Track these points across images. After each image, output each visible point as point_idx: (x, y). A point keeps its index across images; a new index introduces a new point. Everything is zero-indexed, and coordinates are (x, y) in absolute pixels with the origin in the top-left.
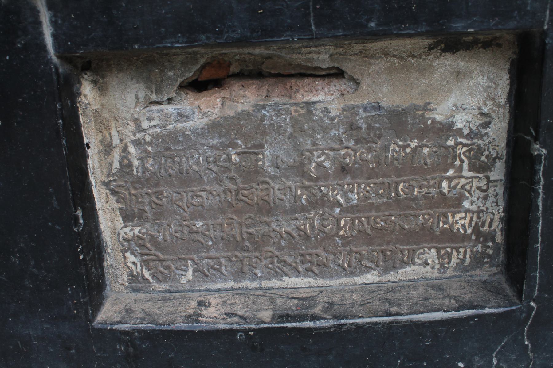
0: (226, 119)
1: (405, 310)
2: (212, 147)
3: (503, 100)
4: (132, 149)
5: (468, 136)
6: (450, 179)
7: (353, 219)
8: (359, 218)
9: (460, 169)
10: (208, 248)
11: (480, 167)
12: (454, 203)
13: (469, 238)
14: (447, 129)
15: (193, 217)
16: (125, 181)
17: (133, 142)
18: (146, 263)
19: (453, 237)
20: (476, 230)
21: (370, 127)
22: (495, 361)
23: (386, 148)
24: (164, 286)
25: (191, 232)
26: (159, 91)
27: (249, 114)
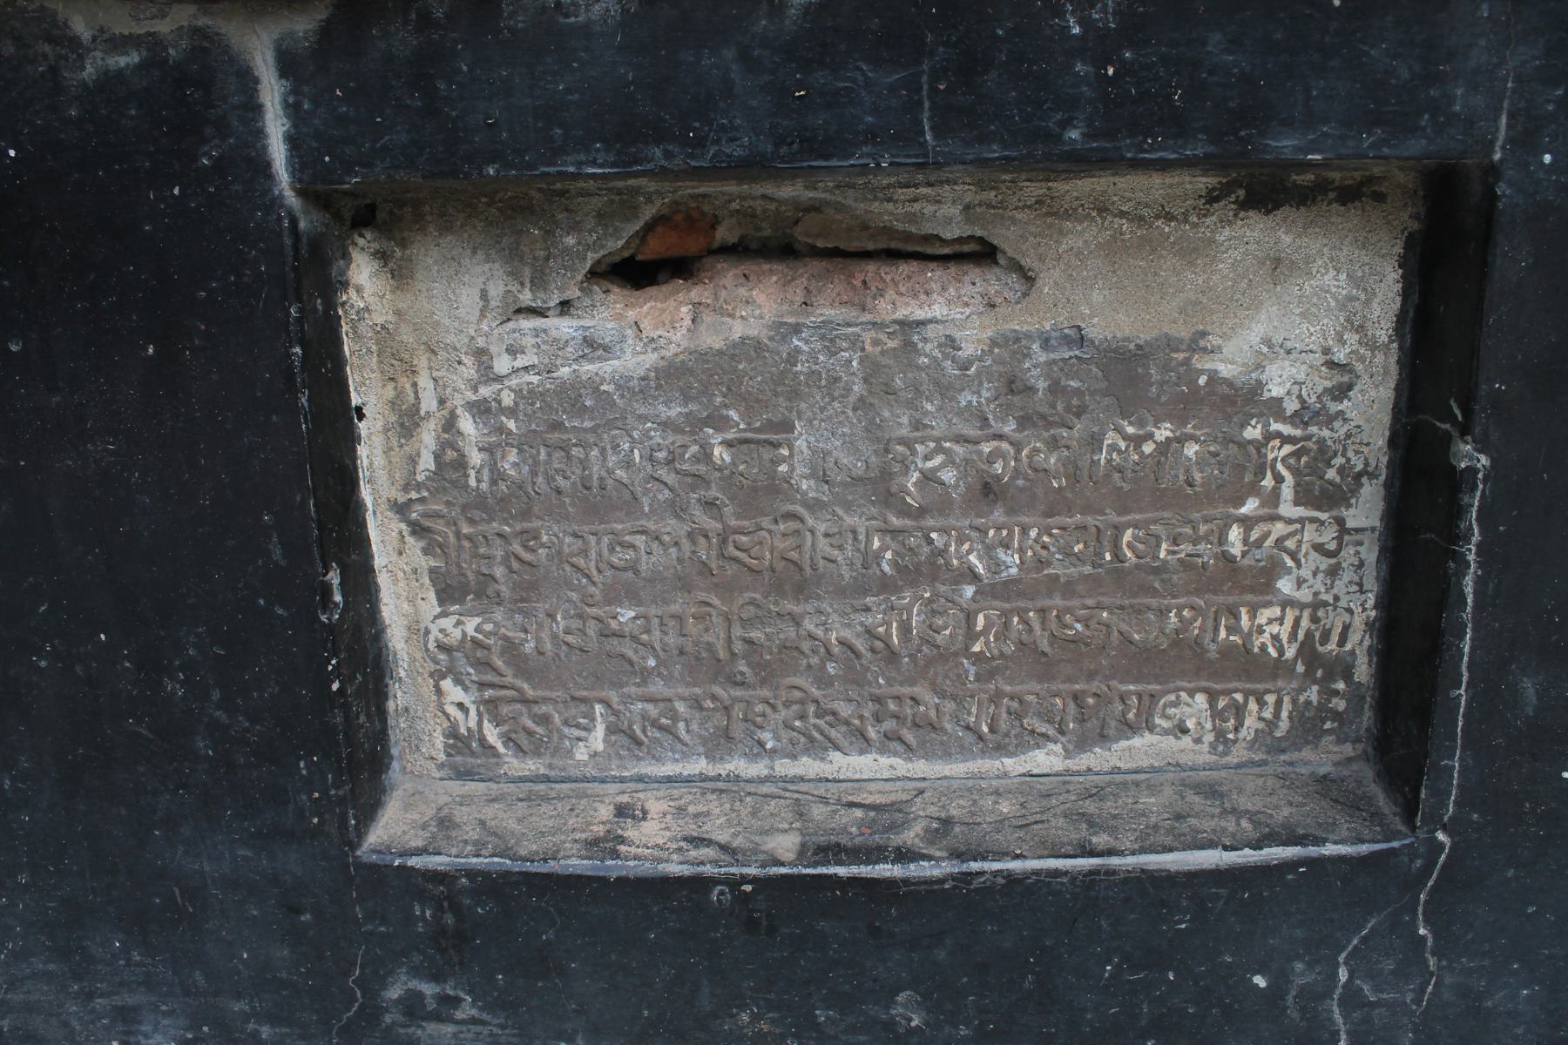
0: (702, 355)
1: (1127, 842)
3: (1383, 331)
5: (1296, 419)
6: (1247, 523)
7: (1006, 614)
8: (1022, 613)
9: (1274, 497)
10: (645, 675)
11: (1324, 496)
13: (1289, 668)
14: (1245, 399)
16: (479, 533)
17: (472, 407)
18: (491, 707)
19: (1248, 665)
20: (1308, 651)
21: (1055, 389)
22: (1343, 974)
23: (1095, 442)
24: (532, 766)
27: (758, 346)
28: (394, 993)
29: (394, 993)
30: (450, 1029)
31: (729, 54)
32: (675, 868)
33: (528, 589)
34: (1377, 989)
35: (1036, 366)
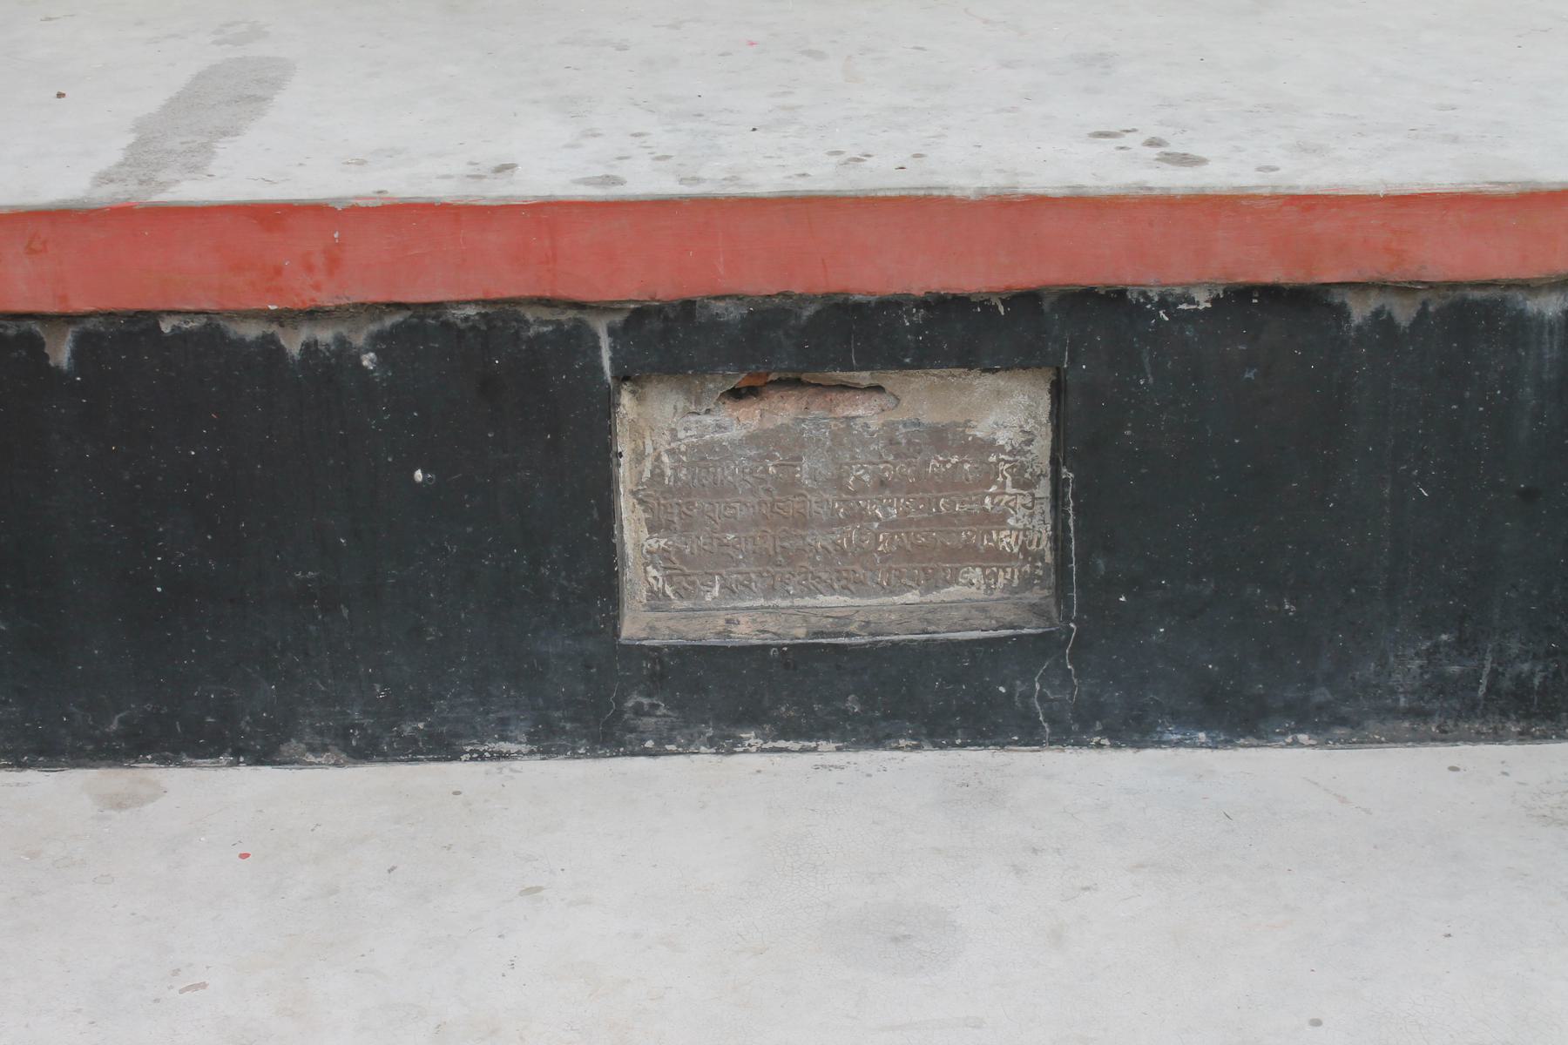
0: (765, 431)
1: (942, 628)
2: (749, 458)
3: (1044, 418)
4: (665, 459)
5: (1010, 453)
6: (993, 496)
7: (892, 535)
8: (899, 534)
9: (1003, 485)
10: (738, 563)
11: (1025, 485)
12: (1000, 520)
13: (1016, 557)
14: (989, 446)
15: (725, 529)
16: (654, 493)
17: (667, 451)
18: (669, 579)
19: (998, 556)
20: (1023, 549)
21: (909, 442)
22: (1038, 687)
23: (926, 464)
24: (686, 604)
25: (721, 545)
26: (698, 402)
27: (788, 427)
28: (630, 704)
29: (630, 704)
30: (653, 720)
31: (781, 333)
32: (755, 641)
33: (687, 527)
34: (1053, 693)
35: (901, 434)
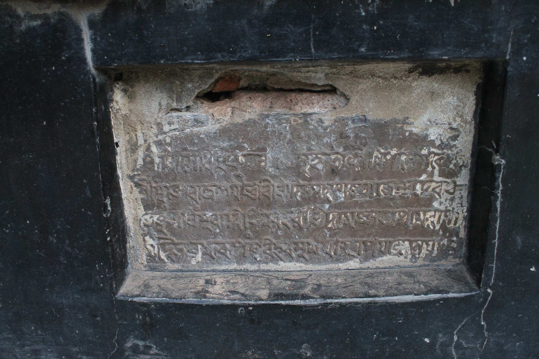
0: (235, 125)
1: (381, 293)
2: (222, 149)
3: (469, 117)
5: (439, 147)
6: (423, 183)
7: (340, 214)
8: (345, 214)
9: (432, 174)
10: (216, 235)
11: (449, 174)
12: (426, 203)
13: (437, 233)
14: (422, 140)
15: (204, 208)
16: (148, 176)
18: (162, 246)
19: (423, 232)
20: (443, 227)
21: (357, 137)
22: (455, 338)
23: (370, 155)
24: (176, 266)
26: (179, 100)
27: (254, 122)
28: (129, 345)
29: (129, 345)
31: (244, 22)
32: (226, 302)
34: (467, 343)
35: (350, 129)
